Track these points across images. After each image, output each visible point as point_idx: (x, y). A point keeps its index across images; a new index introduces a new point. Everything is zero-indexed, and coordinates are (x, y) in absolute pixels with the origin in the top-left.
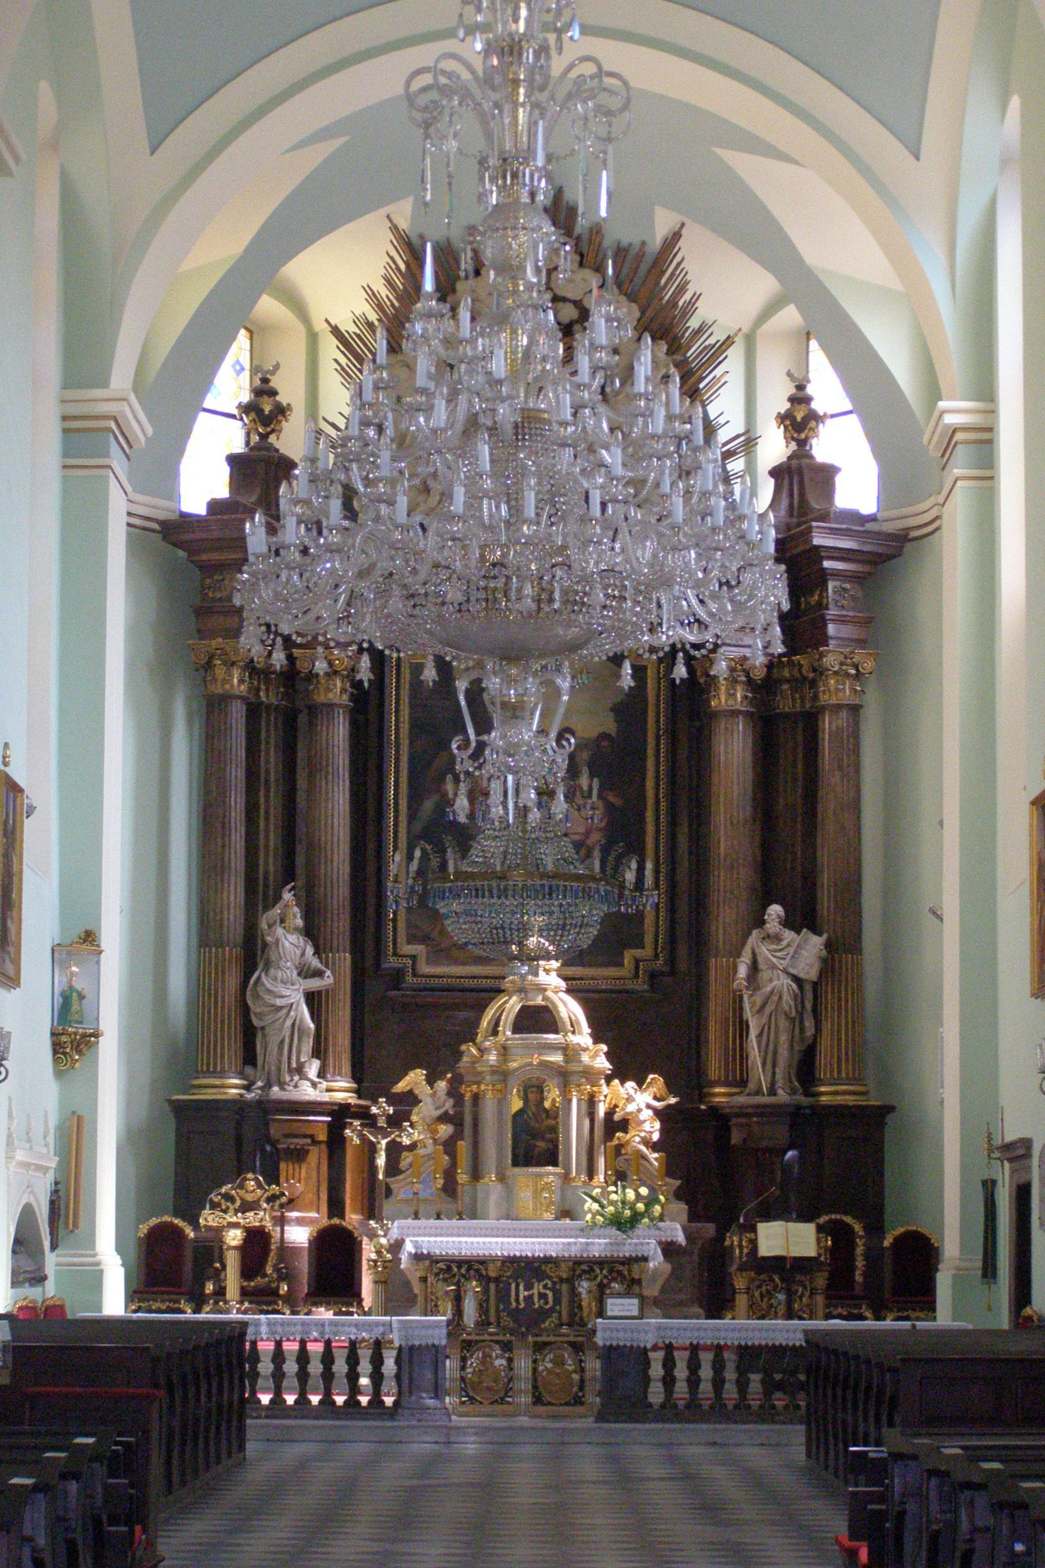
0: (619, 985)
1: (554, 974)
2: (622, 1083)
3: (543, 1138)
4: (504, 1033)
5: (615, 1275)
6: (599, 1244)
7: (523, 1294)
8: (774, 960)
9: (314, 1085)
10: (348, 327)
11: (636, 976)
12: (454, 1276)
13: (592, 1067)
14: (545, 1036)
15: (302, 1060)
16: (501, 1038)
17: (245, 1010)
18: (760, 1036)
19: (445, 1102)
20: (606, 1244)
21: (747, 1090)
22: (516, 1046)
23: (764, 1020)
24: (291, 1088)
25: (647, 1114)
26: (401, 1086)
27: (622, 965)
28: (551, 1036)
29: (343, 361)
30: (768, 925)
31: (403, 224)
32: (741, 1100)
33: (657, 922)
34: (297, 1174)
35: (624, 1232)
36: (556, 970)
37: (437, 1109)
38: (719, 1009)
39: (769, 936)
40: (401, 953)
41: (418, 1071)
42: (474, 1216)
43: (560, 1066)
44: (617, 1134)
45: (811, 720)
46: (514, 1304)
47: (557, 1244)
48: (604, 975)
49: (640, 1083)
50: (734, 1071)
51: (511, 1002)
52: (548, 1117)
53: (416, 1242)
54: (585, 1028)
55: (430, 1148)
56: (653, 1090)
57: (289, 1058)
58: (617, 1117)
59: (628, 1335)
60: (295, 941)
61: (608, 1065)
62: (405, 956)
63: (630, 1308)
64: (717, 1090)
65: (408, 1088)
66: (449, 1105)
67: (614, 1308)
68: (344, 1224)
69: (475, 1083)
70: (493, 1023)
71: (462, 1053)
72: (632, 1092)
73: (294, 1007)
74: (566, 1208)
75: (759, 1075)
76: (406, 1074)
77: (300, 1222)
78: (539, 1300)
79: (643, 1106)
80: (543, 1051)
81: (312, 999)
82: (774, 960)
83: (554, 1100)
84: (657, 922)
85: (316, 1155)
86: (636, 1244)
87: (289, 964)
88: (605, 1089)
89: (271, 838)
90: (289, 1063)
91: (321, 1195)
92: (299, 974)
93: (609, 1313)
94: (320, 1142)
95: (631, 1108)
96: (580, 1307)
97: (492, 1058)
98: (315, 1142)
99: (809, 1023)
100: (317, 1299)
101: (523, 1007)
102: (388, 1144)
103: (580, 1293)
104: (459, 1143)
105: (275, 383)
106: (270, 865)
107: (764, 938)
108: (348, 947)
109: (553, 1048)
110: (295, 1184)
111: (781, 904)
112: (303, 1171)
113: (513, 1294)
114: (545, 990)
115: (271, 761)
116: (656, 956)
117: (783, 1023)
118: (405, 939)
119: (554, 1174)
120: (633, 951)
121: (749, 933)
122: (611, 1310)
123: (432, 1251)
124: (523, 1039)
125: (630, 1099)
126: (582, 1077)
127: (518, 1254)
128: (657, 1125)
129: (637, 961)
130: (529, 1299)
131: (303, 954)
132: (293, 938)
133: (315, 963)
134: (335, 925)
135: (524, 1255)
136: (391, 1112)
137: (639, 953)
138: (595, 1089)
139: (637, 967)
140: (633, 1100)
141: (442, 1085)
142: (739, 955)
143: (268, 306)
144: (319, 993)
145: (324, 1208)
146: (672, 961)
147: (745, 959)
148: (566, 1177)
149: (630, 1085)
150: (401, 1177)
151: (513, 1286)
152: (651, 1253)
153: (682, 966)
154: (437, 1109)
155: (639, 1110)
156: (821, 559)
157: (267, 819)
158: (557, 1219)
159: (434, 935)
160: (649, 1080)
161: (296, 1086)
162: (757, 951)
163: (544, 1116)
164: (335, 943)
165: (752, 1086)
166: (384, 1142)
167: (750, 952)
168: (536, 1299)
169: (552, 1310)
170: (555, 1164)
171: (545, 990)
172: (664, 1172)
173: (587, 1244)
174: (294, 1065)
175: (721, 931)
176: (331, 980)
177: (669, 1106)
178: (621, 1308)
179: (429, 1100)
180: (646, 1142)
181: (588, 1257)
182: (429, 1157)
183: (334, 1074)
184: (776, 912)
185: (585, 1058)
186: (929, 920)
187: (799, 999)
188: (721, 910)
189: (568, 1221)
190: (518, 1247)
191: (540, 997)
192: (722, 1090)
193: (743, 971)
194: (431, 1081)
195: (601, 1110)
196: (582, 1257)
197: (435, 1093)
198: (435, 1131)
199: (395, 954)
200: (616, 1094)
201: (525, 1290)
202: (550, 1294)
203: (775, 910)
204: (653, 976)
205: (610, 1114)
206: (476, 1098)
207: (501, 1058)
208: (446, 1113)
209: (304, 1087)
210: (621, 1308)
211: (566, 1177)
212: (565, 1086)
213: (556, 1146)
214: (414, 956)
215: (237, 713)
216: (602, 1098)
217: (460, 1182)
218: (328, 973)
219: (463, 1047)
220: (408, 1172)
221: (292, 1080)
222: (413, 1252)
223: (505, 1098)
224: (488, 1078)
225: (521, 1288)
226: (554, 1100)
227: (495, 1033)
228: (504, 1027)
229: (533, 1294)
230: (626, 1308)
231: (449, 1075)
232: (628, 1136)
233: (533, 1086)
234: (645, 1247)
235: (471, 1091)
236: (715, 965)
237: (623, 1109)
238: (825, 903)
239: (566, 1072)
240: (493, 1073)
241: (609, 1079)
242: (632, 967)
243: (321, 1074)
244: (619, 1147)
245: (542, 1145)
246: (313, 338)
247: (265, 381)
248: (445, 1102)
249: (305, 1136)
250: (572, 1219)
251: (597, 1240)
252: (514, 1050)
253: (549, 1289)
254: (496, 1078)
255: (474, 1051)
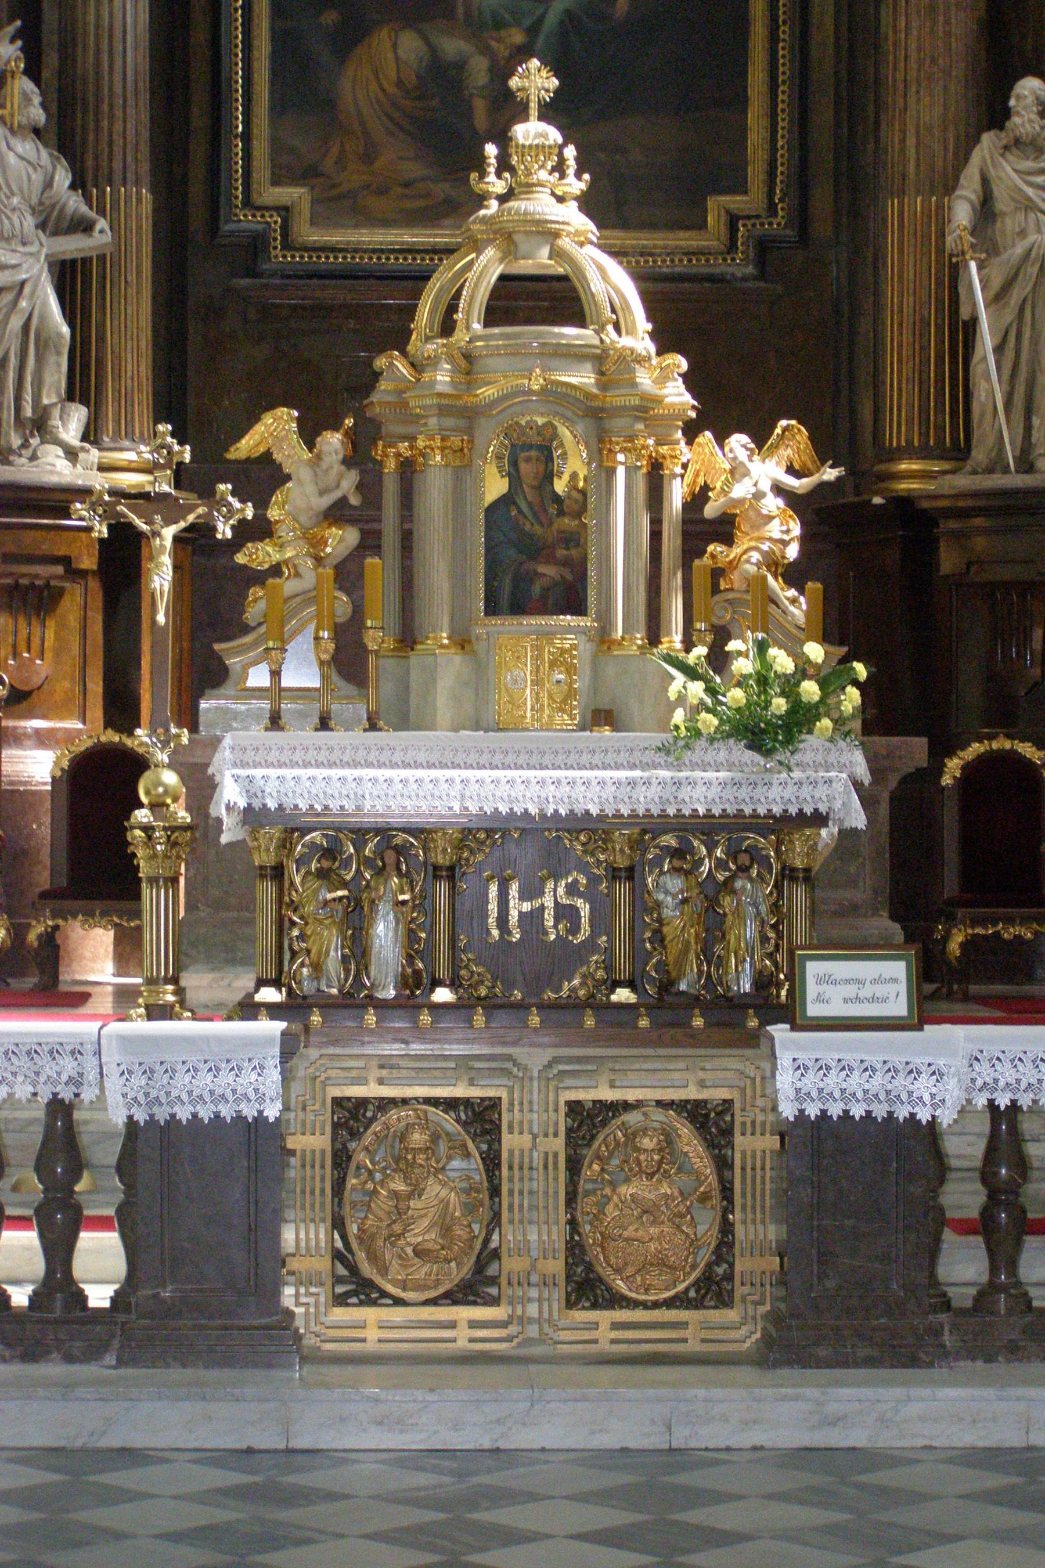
0: (698, 265)
1: (574, 205)
2: (721, 439)
3: (551, 559)
4: (468, 328)
5: (744, 859)
6: (707, 784)
7: (517, 907)
8: (1030, 192)
9: (71, 454)
11: (732, 247)
12: (346, 864)
13: (658, 400)
14: (556, 330)
15: (46, 401)
16: (461, 337)
18: (999, 349)
19: (341, 476)
20: (723, 784)
21: (969, 465)
22: (496, 353)
23: (1009, 315)
24: (23, 460)
25: (773, 504)
26: (247, 446)
27: (702, 225)
28: (570, 332)
30: (1016, 120)
32: (963, 482)
33: (773, 141)
34: (36, 642)
35: (767, 753)
36: (577, 199)
37: (322, 493)
38: (909, 301)
39: (1017, 142)
40: (258, 201)
41: (282, 411)
42: (403, 722)
43: (588, 396)
44: (711, 548)
46: (495, 933)
47: (602, 783)
49: (760, 439)
50: (940, 429)
51: (483, 259)
52: (561, 513)
53: (250, 779)
54: (643, 325)
55: (309, 579)
56: (786, 453)
57: (18, 398)
58: (710, 511)
59: (878, 1082)
60: (32, 155)
61: (688, 399)
62: (267, 208)
63: (881, 990)
64: (903, 466)
65: (262, 449)
66: (348, 482)
67: (828, 990)
68: (129, 742)
69: (404, 438)
70: (442, 308)
71: (377, 375)
72: (742, 455)
73: (27, 290)
74: (604, 703)
76: (258, 419)
77: (43, 739)
78: (557, 920)
79: (765, 486)
80: (554, 363)
82: (1030, 192)
83: (574, 476)
84: (773, 141)
85: (79, 599)
86: (799, 784)
87: (15, 200)
88: (685, 452)
90: (18, 409)
91: (90, 685)
92: (42, 226)
93: (814, 1010)
94: (83, 574)
95: (741, 490)
96: (659, 938)
97: (443, 377)
98: (75, 574)
100: (68, 904)
101: (502, 278)
102: (177, 539)
103: (658, 905)
104: (369, 561)
107: (1006, 148)
108: (145, 167)
109: (575, 355)
110: (31, 660)
111: (741, 431)
112: (50, 635)
113: (493, 907)
114: (556, 235)
116: (772, 209)
118: (268, 175)
119: (577, 631)
120: (723, 199)
121: (977, 140)
122: (819, 999)
123: (288, 803)
124: (507, 337)
125: (737, 472)
126: (637, 419)
127: (504, 809)
128: (796, 529)
129: (733, 220)
130: (532, 920)
131: (48, 184)
132: (27, 147)
133: (75, 203)
134: (118, 127)
135: (518, 810)
136: (187, 457)
137: (736, 202)
138: (664, 450)
139: (733, 229)
140: (747, 473)
141: (333, 441)
142: (950, 186)
144: (86, 261)
145: (96, 711)
146: (802, 218)
147: (969, 189)
148: (603, 638)
149: (739, 442)
150: (248, 639)
151: (493, 890)
152: (837, 805)
153: (822, 229)
154: (322, 493)
155: (759, 496)
158: (582, 728)
159: (328, 165)
160: (778, 430)
161: (33, 457)
162: (992, 173)
163: (552, 510)
164: (117, 165)
165: (979, 455)
166: (169, 533)
167: (977, 177)
168: (549, 922)
169: (590, 945)
170: (578, 608)
171: (556, 235)
173: (678, 783)
174: (28, 412)
175: (911, 142)
176: (108, 237)
177: (822, 485)
178: (851, 990)
179: (304, 474)
180: (772, 563)
181: (679, 815)
182: (310, 598)
183: (117, 435)
184: (1033, 92)
185: (644, 379)
188: (912, 99)
189: (607, 732)
190: (503, 790)
191: (545, 251)
192: (915, 466)
193: (962, 214)
194: (309, 434)
195: (677, 494)
196: (663, 815)
197: (319, 457)
198: (316, 543)
199: (247, 203)
200: (710, 467)
201: (523, 897)
202: (584, 909)
204: (764, 247)
205: (698, 498)
206: (408, 469)
207: (461, 378)
208: (343, 501)
209: (50, 459)
210: (851, 990)
211: (603, 638)
212: (601, 440)
213: (583, 577)
214: (286, 209)
216: (678, 470)
217: (372, 646)
218: (102, 224)
219: (380, 362)
220: (263, 629)
221: (25, 445)
222: (242, 803)
223: (468, 466)
224: (433, 422)
225: (514, 889)
226: (574, 476)
227: (447, 328)
228: (468, 313)
229: (542, 908)
230: (867, 992)
231: (349, 422)
232: (736, 551)
233: (530, 447)
234: (822, 792)
235: (398, 455)
237: (724, 492)
239: (602, 410)
240: (443, 411)
241: (691, 432)
242: (724, 231)
243: (91, 435)
244: (717, 573)
245: (549, 571)
248: (341, 476)
249: (55, 560)
250: (616, 728)
251: (698, 774)
252: (492, 362)
253: (580, 895)
254: (450, 422)
255: (402, 367)
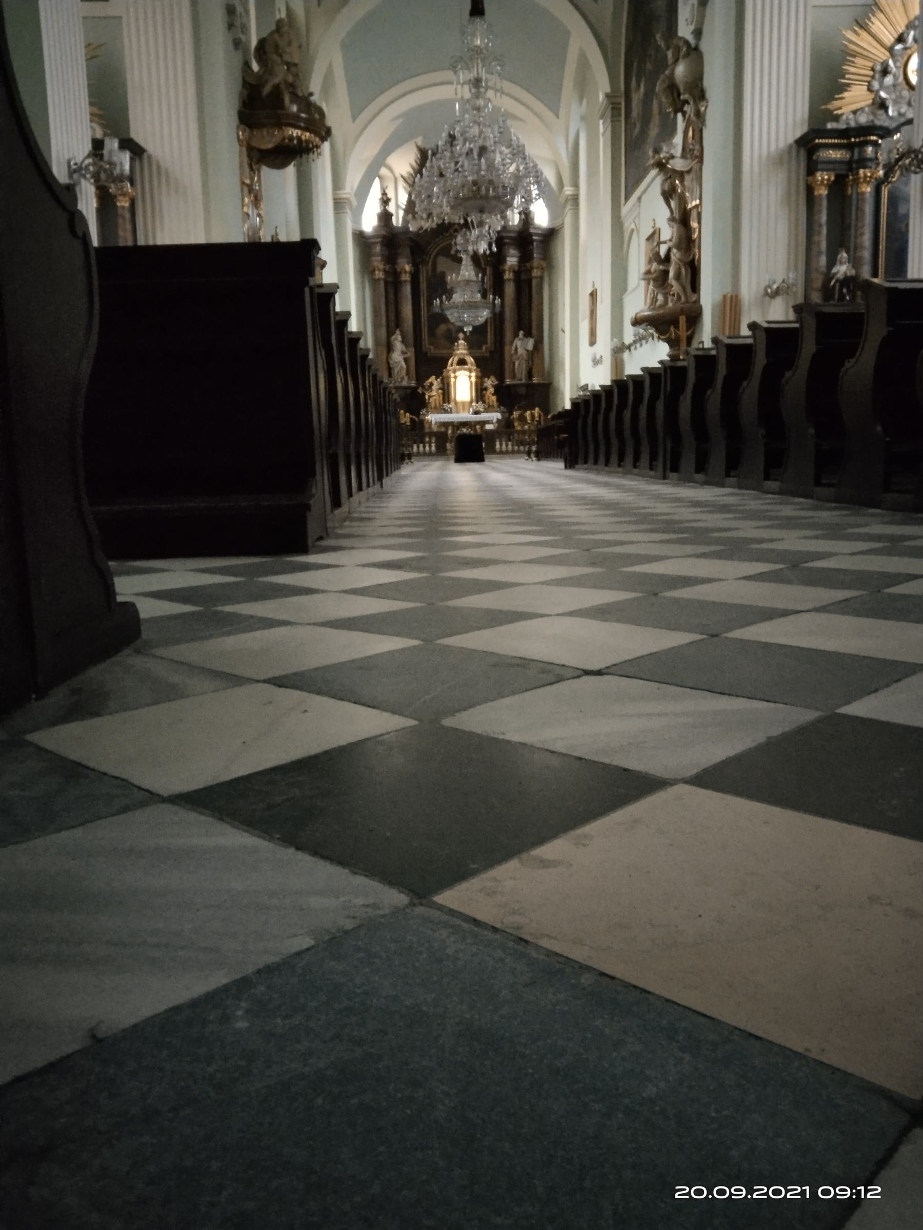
10: (405, 175)
17: (388, 363)
25: (490, 387)
29: (405, 185)
31: (420, 144)
45: (529, 281)
48: (478, 353)
66: (441, 385)
75: (518, 375)
81: (406, 360)
89: (392, 318)
99: (530, 363)
105: (387, 191)
106: (392, 324)
115: (392, 296)
117: (524, 362)
137: (487, 346)
141: (439, 380)
143: (384, 171)
156: (532, 236)
157: (380, 394)
172: (444, 455)
186: (561, 332)
187: (528, 355)
194: (436, 379)
203: (521, 333)
204: (491, 352)
215: (382, 284)
236: (507, 348)
238: (534, 331)
246: (396, 180)
247: (384, 191)
